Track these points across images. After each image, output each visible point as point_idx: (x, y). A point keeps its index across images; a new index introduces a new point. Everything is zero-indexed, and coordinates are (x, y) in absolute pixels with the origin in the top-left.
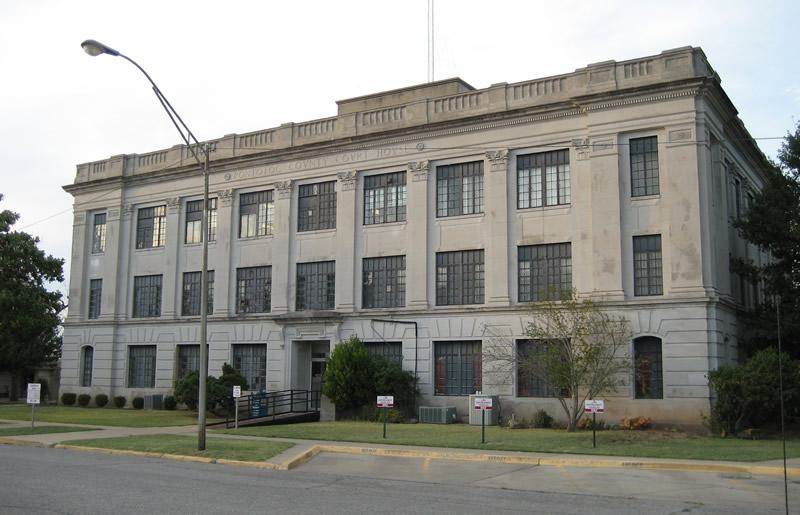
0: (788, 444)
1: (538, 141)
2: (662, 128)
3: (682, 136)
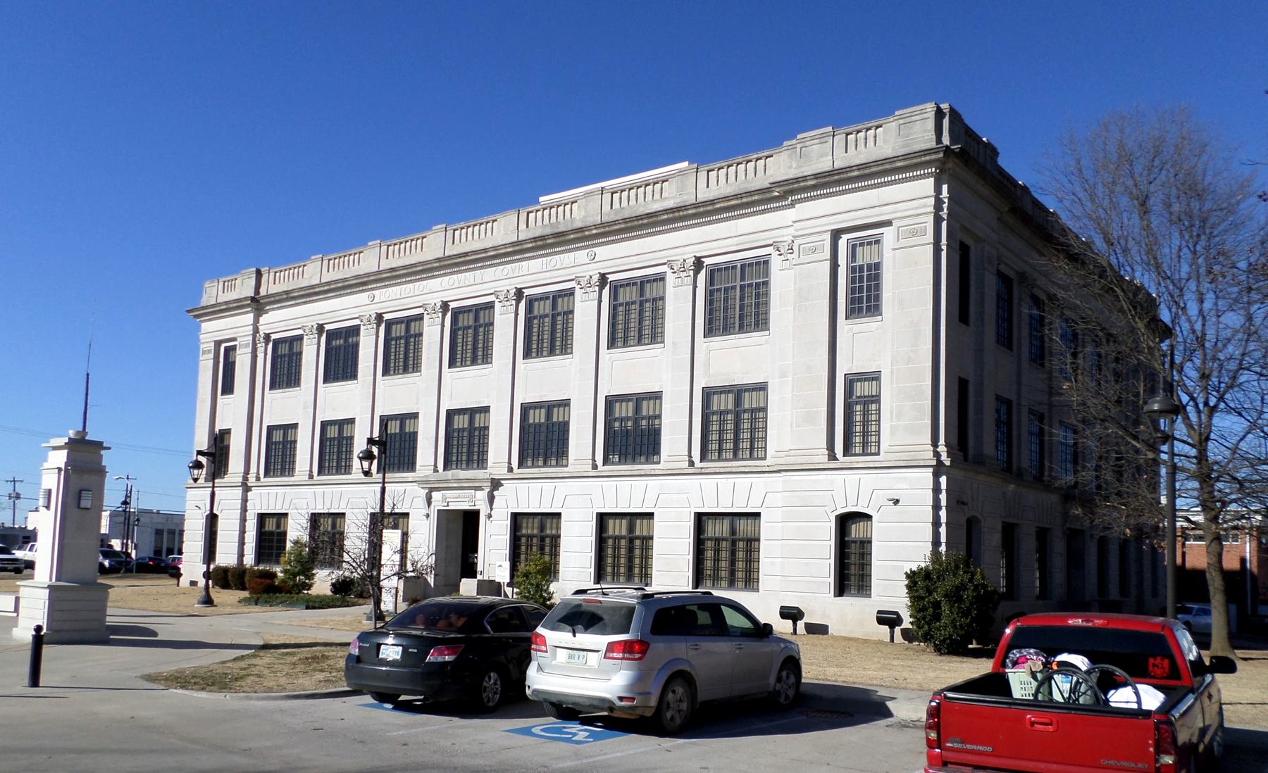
0: (8, 524)
1: (731, 244)
2: (888, 223)
3: (915, 234)
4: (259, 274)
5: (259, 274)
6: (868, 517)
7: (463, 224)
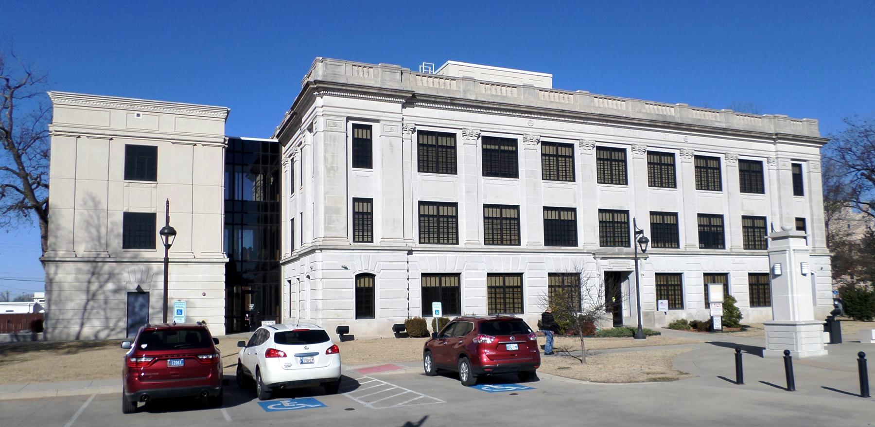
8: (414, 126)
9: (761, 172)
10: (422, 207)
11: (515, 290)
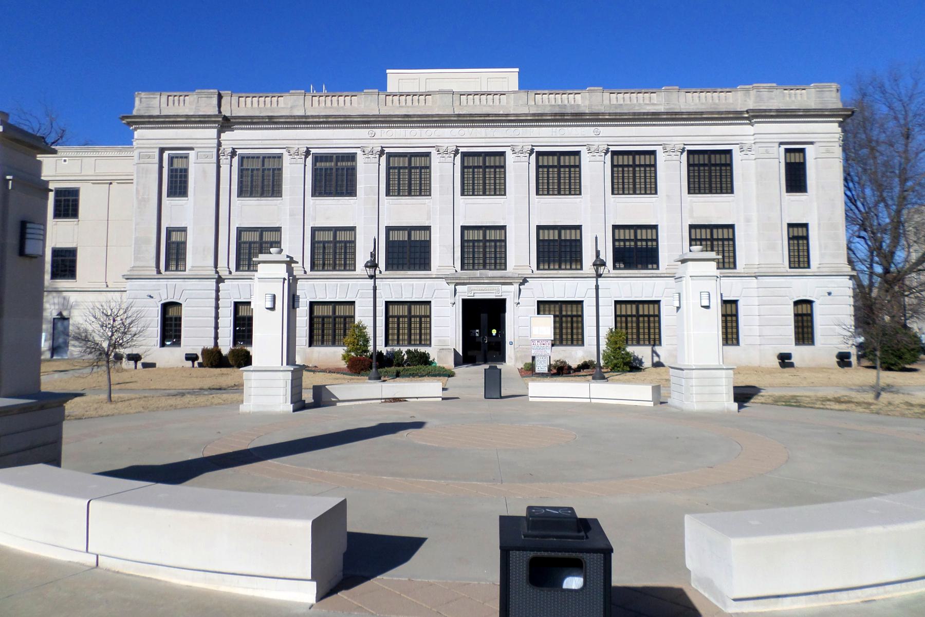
4: (220, 97)
5: (220, 97)
6: (179, 305)
7: (178, 94)
8: (682, 146)
9: (729, 165)
10: (693, 231)
11: (805, 318)
